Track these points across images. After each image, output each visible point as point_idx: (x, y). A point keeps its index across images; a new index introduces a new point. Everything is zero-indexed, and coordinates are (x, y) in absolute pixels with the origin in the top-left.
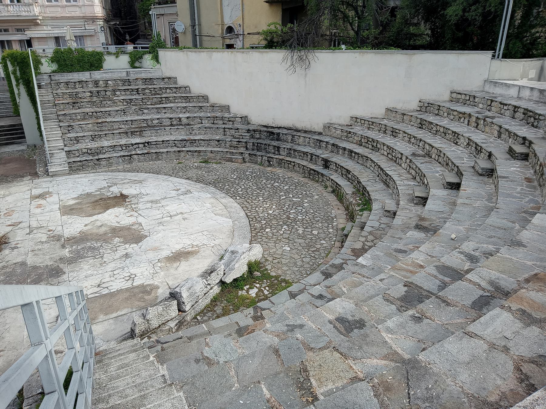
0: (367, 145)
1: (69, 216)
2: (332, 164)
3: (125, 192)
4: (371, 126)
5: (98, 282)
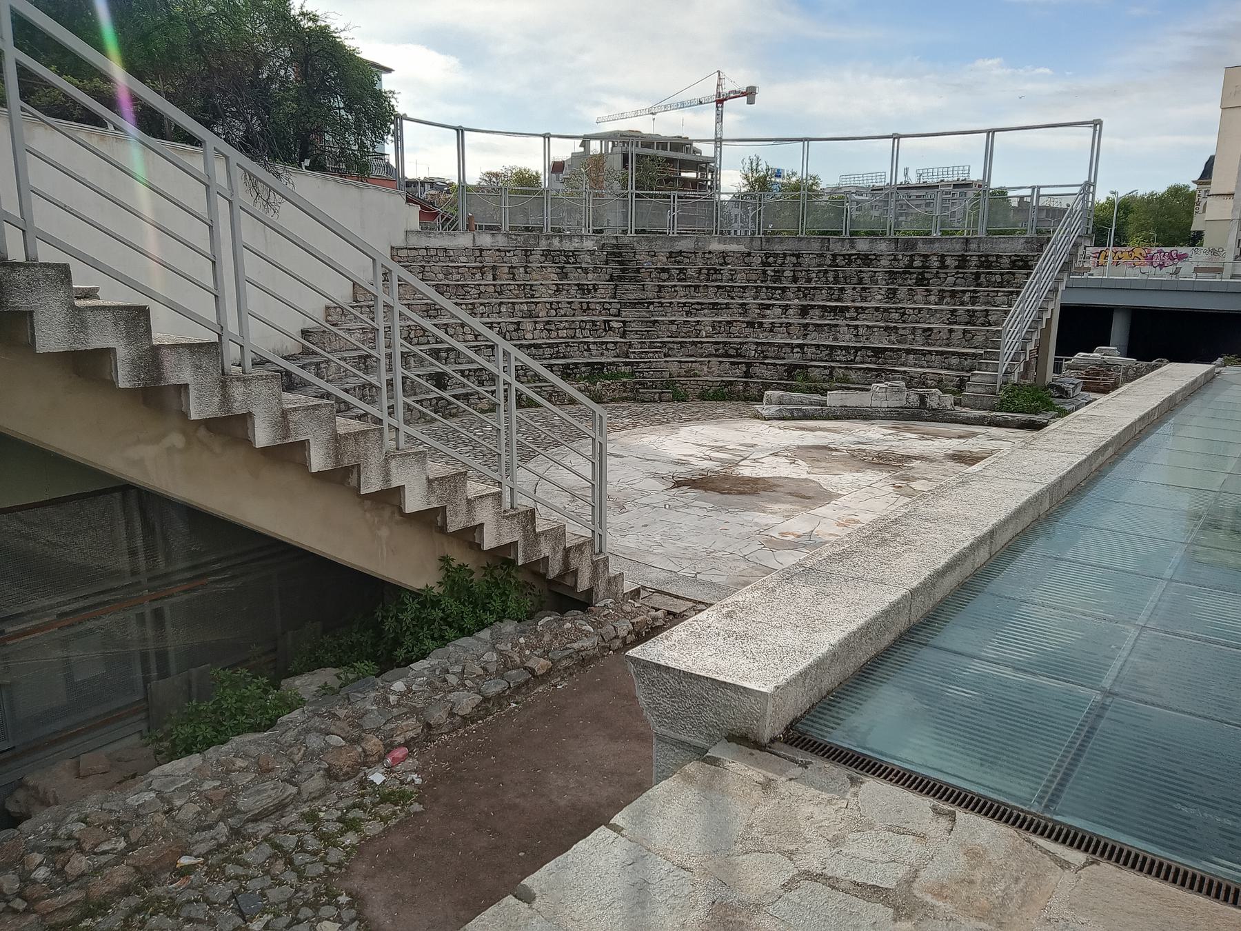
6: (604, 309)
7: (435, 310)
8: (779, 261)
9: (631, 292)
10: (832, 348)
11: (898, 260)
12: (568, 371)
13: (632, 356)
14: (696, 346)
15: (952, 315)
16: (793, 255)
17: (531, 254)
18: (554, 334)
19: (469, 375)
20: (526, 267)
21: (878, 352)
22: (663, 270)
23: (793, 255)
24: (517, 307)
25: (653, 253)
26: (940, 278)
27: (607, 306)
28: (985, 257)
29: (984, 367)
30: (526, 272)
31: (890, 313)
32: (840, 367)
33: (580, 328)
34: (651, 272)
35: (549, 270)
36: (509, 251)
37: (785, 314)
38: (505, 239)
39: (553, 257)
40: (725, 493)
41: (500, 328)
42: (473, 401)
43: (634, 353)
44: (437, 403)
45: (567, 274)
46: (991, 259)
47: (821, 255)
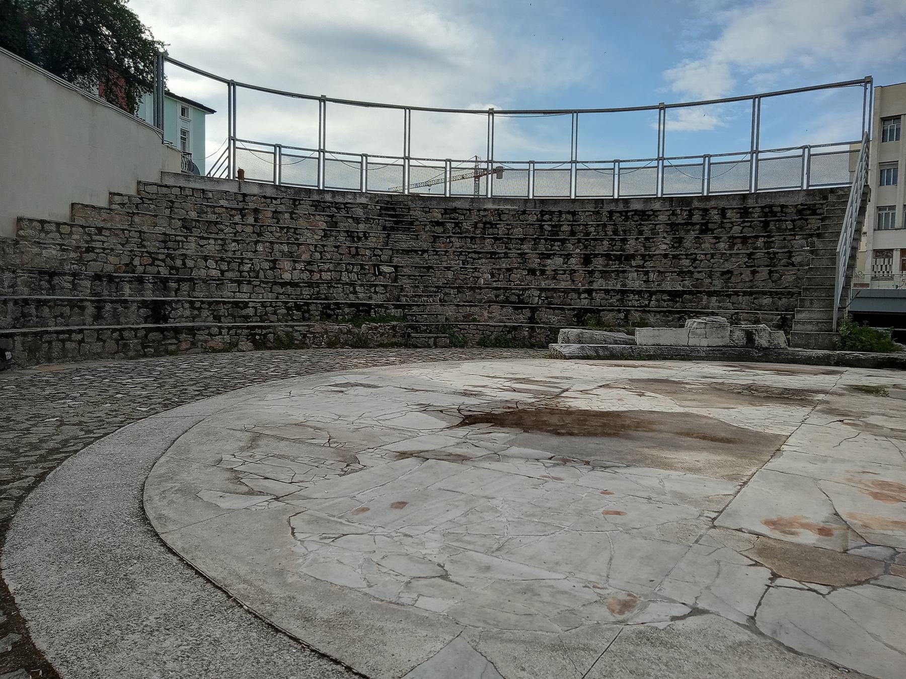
2: (179, 305)
6: (375, 255)
7: (175, 241)
8: (555, 219)
9: (403, 241)
10: (623, 292)
12: (329, 311)
13: (404, 299)
14: (475, 292)
15: (749, 259)
16: (569, 212)
17: (300, 204)
20: (292, 213)
21: (674, 295)
22: (438, 224)
23: (569, 212)
24: (276, 246)
26: (725, 228)
28: (768, 208)
30: (292, 218)
31: (680, 259)
34: (425, 225)
35: (318, 218)
36: (276, 199)
40: (563, 434)
41: (252, 264)
42: (201, 338)
44: (146, 336)
45: (336, 223)
46: (776, 209)
47: (598, 213)
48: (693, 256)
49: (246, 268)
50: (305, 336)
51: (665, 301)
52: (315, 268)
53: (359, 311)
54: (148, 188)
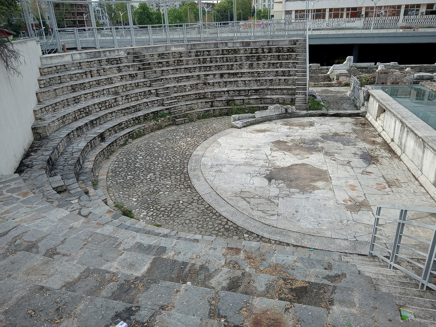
0: (81, 116)
1: (321, 168)
3: (266, 182)
4: (56, 108)
5: (304, 130)
6: (145, 84)
8: (202, 54)
11: (247, 51)
15: (276, 73)
16: (207, 51)
17: (102, 62)
18: (130, 100)
19: (111, 130)
25: (152, 55)
27: (145, 83)
29: (298, 94)
30: (104, 71)
32: (246, 99)
33: (140, 95)
35: (114, 69)
37: (214, 77)
38: (86, 55)
39: (111, 62)
41: (109, 102)
43: (167, 103)
45: (121, 70)
46: (280, 49)
48: (258, 72)
49: (107, 104)
50: (144, 130)
51: (253, 93)
52: (129, 97)
53: (155, 114)
54: (45, 70)
